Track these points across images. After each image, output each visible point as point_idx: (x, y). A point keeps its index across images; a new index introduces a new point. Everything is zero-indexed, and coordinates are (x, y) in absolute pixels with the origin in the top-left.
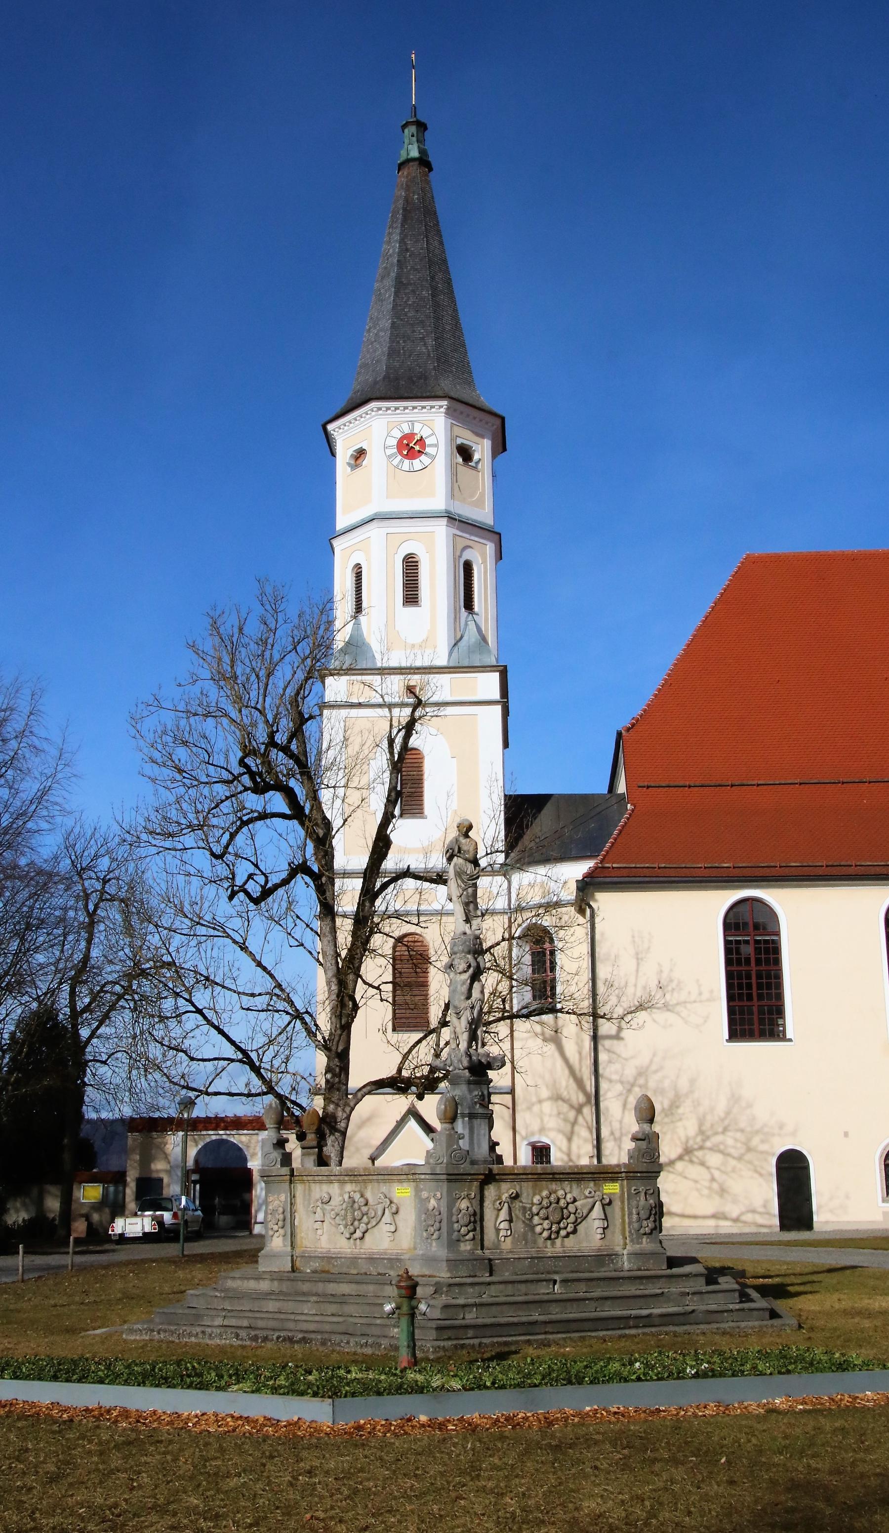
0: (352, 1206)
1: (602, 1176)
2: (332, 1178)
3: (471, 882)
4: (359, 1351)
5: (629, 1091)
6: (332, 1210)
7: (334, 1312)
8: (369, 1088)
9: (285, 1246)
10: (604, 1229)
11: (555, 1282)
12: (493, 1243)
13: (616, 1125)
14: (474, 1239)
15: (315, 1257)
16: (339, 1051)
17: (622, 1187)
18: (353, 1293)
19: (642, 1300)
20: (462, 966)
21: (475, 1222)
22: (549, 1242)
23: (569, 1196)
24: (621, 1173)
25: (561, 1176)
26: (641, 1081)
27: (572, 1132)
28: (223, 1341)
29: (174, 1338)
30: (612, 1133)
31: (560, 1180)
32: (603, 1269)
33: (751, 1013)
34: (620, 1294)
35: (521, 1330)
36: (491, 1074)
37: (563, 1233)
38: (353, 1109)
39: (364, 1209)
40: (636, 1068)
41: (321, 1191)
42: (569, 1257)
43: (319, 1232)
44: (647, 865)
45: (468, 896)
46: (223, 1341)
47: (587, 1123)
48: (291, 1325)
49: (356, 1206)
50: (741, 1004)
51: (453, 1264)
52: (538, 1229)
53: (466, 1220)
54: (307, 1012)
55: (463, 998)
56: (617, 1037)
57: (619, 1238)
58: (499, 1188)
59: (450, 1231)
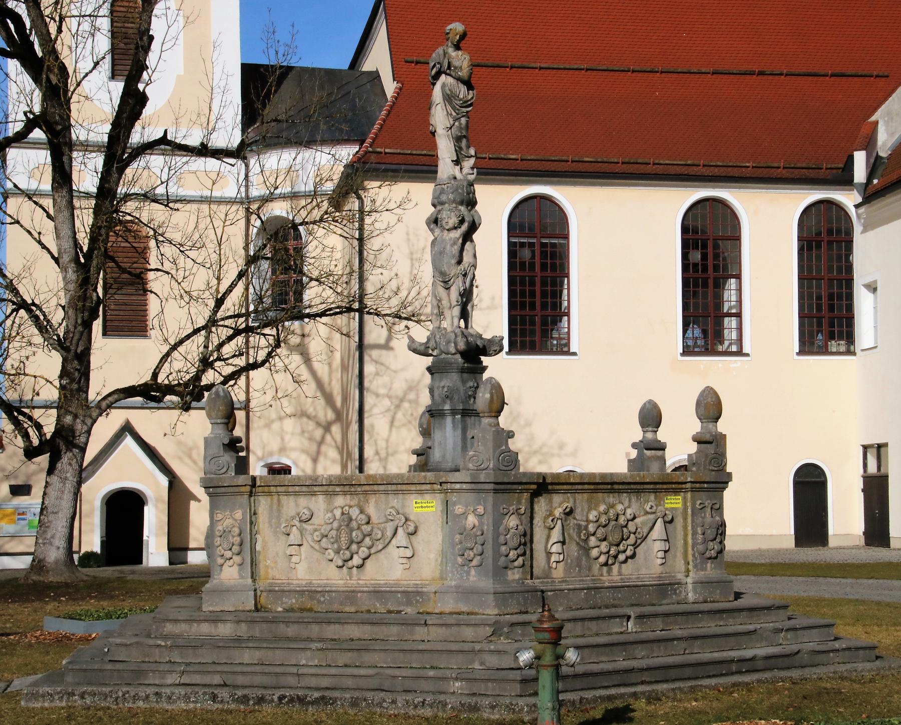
0: (348, 525)
1: (665, 486)
2: (316, 489)
3: (464, 110)
4: (412, 712)
5: (398, 407)
6: (316, 530)
7: (348, 662)
8: (116, 396)
9: (242, 577)
10: (666, 552)
11: (629, 618)
12: (544, 570)
13: (382, 444)
14: (523, 565)
15: (289, 591)
16: (79, 351)
17: (685, 499)
18: (366, 637)
19: (732, 639)
20: (453, 221)
21: (525, 544)
22: (605, 568)
23: (629, 511)
24: (686, 483)
25: (621, 487)
26: (412, 396)
27: (318, 452)
28: (192, 706)
29: (109, 703)
30: (377, 453)
31: (619, 492)
32: (664, 602)
33: (533, 323)
34: (699, 632)
35: (616, 679)
36: (485, 360)
37: (622, 557)
38: (95, 421)
39: (366, 529)
40: (406, 381)
41: (297, 505)
42: (628, 586)
43: (295, 559)
44: (424, 152)
45: (460, 128)
46: (192, 706)
47: (336, 442)
48: (292, 681)
49: (354, 524)
50: (523, 313)
51: (502, 597)
52: (594, 553)
53: (516, 542)
54: (33, 304)
55: (453, 261)
56: (386, 346)
57: (680, 565)
58: (551, 501)
59: (497, 554)
